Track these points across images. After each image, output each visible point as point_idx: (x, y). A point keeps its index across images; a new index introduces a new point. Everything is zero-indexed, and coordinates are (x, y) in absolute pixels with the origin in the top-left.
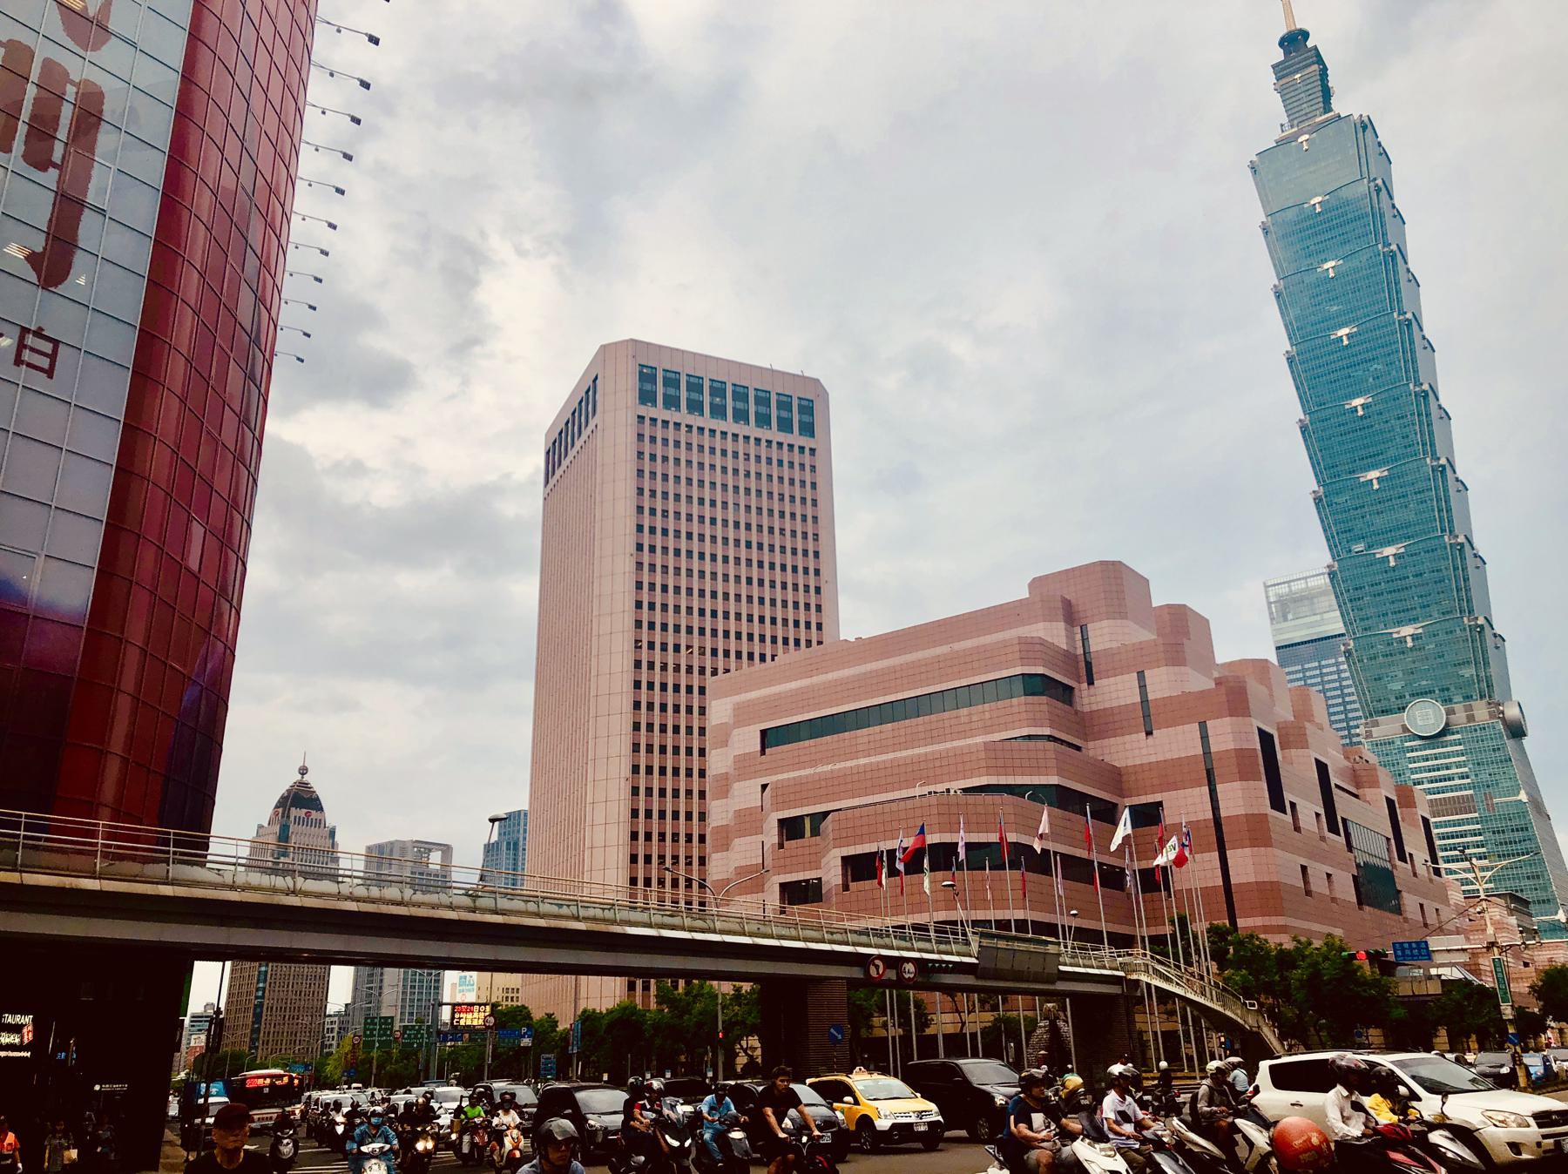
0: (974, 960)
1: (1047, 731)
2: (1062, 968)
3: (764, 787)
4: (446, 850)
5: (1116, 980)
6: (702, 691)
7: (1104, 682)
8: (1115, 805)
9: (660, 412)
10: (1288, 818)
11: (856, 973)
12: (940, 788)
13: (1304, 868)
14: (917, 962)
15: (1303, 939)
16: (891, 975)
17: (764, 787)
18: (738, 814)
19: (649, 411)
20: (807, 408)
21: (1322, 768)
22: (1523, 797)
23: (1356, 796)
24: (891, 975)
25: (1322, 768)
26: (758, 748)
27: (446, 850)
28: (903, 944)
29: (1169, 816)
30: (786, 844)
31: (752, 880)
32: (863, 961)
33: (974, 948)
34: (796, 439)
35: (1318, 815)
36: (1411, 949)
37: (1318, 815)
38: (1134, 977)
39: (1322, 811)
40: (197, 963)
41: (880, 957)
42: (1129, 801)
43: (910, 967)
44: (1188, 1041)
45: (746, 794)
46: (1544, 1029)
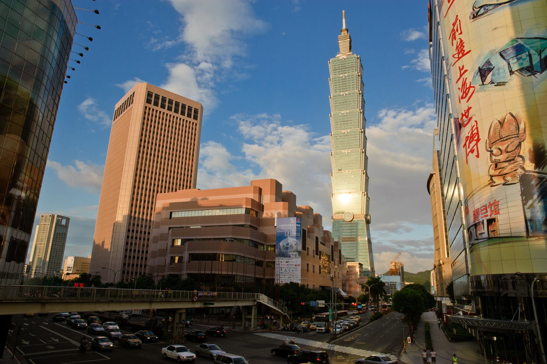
4: (68, 219)
9: (152, 106)
10: (306, 252)
19: (148, 105)
20: (196, 111)
21: (317, 238)
22: (366, 239)
25: (317, 238)
34: (192, 120)
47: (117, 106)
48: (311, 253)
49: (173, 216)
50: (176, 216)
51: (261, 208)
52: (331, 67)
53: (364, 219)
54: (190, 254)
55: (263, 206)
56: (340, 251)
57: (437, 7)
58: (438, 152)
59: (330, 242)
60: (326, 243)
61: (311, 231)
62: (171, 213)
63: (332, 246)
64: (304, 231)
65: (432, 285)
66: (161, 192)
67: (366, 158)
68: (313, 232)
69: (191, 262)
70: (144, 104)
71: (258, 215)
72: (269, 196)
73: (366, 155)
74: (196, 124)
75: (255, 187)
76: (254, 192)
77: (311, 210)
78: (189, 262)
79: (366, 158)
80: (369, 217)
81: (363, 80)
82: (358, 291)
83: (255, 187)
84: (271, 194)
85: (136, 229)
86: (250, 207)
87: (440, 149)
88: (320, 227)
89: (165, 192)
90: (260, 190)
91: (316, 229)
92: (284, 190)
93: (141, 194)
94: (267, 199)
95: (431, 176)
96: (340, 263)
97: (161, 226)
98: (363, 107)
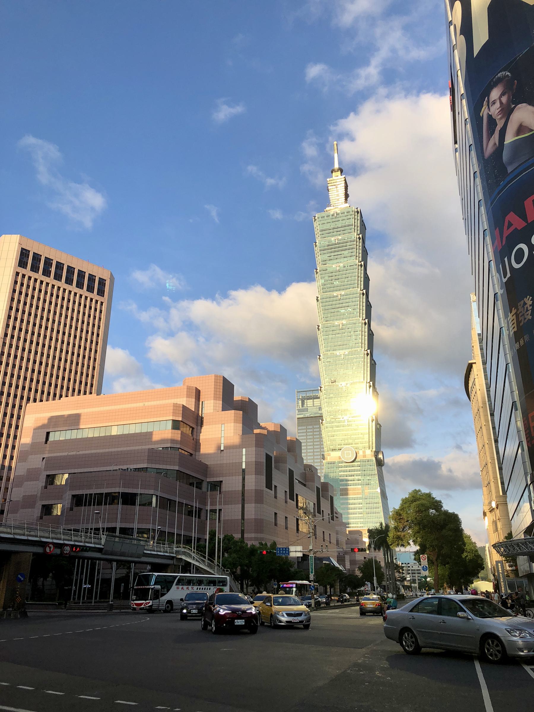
0: (102, 547)
1: (12, 477)
2: (145, 552)
3: (44, 458)
5: (173, 558)
6: (20, 407)
7: (208, 427)
8: (203, 481)
9: (28, 272)
11: (40, 550)
12: (125, 467)
13: (276, 514)
14: (72, 546)
15: (264, 543)
16: (58, 551)
17: (44, 458)
18: (29, 470)
19: (22, 271)
20: (102, 282)
21: (291, 473)
23: (305, 485)
24: (58, 551)
26: (44, 440)
28: (67, 537)
29: (224, 488)
30: (44, 517)
31: (28, 502)
32: (44, 545)
33: (103, 541)
34: (95, 296)
35: (286, 492)
36: (283, 550)
37: (286, 492)
38: (180, 557)
39: (288, 491)
40: (234, 399)
41: (53, 544)
42: (208, 480)
43: (68, 548)
44: (76, 585)
46: (364, 585)
48: (281, 495)
49: (51, 438)
50: (57, 439)
51: (199, 421)
53: (374, 459)
54: (74, 496)
55: (202, 418)
56: (332, 498)
57: (459, 71)
58: (479, 335)
59: (313, 481)
60: (307, 483)
61: (280, 460)
62: (48, 433)
63: (318, 489)
64: (268, 458)
65: (464, 101)
66: (35, 400)
68: (285, 462)
69: (44, 517)
70: (15, 268)
71: (195, 433)
72: (212, 401)
74: (102, 303)
75: (189, 388)
76: (188, 396)
77: (283, 430)
78: (71, 509)
80: (380, 456)
81: (372, 328)
83: (189, 388)
84: (215, 398)
86: (180, 419)
87: (480, 332)
88: (298, 458)
89: (41, 401)
90: (198, 393)
91: (290, 459)
92: (237, 397)
94: (210, 406)
95: (470, 367)
96: (333, 519)
97: (30, 457)
98: (368, 315)
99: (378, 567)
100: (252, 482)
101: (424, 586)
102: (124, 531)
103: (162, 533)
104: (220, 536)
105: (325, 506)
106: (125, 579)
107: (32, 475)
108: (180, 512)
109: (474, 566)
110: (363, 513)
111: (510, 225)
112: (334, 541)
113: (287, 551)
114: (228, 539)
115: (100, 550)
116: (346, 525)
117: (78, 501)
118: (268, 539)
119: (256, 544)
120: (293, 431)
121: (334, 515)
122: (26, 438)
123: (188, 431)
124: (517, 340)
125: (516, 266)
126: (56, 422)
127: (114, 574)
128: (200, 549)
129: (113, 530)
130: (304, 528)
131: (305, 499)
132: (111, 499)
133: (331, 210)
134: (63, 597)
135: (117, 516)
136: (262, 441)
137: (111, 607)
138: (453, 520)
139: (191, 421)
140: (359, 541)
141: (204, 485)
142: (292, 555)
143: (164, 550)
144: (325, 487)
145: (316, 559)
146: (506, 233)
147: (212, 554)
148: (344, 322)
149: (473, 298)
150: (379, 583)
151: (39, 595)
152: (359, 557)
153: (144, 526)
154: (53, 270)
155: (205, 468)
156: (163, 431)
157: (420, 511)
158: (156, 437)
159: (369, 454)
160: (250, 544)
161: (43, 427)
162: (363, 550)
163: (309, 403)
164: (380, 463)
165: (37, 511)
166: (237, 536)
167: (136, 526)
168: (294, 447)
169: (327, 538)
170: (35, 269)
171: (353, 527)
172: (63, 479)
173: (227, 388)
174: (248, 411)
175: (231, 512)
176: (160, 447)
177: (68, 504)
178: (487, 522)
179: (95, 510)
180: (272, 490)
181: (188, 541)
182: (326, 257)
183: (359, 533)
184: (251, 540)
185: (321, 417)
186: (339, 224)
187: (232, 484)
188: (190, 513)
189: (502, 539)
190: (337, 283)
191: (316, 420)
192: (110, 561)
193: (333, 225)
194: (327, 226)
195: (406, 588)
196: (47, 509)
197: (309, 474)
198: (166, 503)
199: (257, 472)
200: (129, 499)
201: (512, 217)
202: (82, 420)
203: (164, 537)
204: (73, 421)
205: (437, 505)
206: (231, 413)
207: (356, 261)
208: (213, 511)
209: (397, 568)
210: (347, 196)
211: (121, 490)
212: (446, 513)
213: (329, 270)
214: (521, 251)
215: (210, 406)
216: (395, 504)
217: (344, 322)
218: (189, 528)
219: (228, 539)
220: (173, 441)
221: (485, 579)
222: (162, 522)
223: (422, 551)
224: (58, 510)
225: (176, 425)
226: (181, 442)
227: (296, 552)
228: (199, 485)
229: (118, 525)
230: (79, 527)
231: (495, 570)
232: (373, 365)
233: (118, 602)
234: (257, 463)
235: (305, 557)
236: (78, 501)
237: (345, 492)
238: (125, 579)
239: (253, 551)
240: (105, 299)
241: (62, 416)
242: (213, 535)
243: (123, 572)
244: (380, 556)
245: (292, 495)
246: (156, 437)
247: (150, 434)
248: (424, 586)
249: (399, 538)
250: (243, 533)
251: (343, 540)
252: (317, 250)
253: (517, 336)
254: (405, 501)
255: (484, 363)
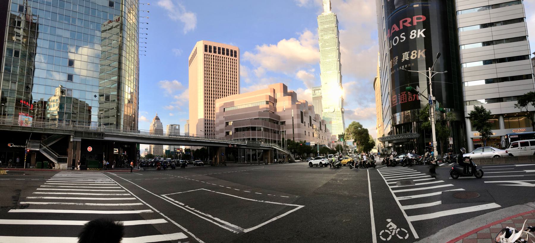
4: (179, 125)
9: (208, 53)
11: (227, 146)
19: (206, 53)
20: (235, 52)
21: (310, 117)
25: (310, 117)
27: (179, 125)
29: (286, 123)
31: (221, 131)
32: (228, 144)
45: (221, 118)
47: (190, 58)
48: (307, 124)
51: (275, 101)
52: (319, 21)
64: (302, 113)
67: (340, 65)
73: (340, 63)
75: (271, 89)
76: (271, 92)
79: (340, 65)
82: (337, 138)
84: (281, 92)
85: (208, 125)
88: (313, 112)
90: (274, 90)
92: (289, 90)
93: (209, 105)
94: (279, 95)
95: (376, 79)
99: (341, 147)
100: (297, 121)
101: (355, 152)
102: (253, 139)
103: (266, 140)
104: (286, 139)
105: (323, 128)
106: (255, 155)
107: (221, 123)
108: (271, 132)
109: (372, 145)
110: (337, 128)
111: (394, 29)
112: (326, 139)
113: (309, 143)
114: (289, 140)
115: (246, 146)
116: (331, 133)
117: (237, 130)
118: (303, 140)
119: (299, 142)
120: (310, 102)
121: (326, 130)
122: (217, 111)
123: (272, 104)
124: (392, 71)
125: (394, 45)
126: (226, 104)
127: (251, 153)
128: (279, 144)
129: (249, 139)
130: (315, 135)
131: (316, 125)
132: (248, 129)
133: (324, 14)
134: (236, 160)
135: (250, 135)
136: (298, 106)
137: (252, 163)
138: (366, 131)
139: (273, 101)
140: (335, 139)
141: (279, 123)
142: (311, 145)
143: (267, 145)
144: (323, 121)
145: (320, 145)
146: (392, 32)
147: (283, 146)
148: (330, 60)
149: (379, 54)
150: (341, 152)
151: (229, 159)
152: (335, 144)
153: (259, 137)
154: (217, 50)
155: (279, 117)
156: (263, 106)
157: (355, 129)
158: (260, 107)
159: (340, 110)
160: (296, 142)
161: (222, 106)
162: (335, 142)
163: (317, 91)
164: (343, 112)
165: (224, 134)
166: (292, 139)
167: (257, 137)
168: (311, 108)
169: (324, 138)
170: (215, 52)
171: (333, 134)
172: (231, 123)
173: (285, 88)
174: (293, 96)
175: (289, 131)
176: (262, 111)
177: (234, 131)
178: (377, 131)
179: (242, 133)
180: (405, 210)
181: (275, 142)
182: (323, 33)
183: (335, 136)
184: (297, 140)
185: (321, 97)
186: (328, 20)
187: (289, 122)
188: (275, 133)
189: (381, 136)
190: (327, 44)
191: (319, 98)
192: (250, 149)
193: (325, 20)
194: (323, 21)
195: (351, 153)
196: (227, 133)
197: (317, 117)
198: (266, 130)
199: (298, 118)
200: (254, 129)
201: (395, 26)
202: (235, 103)
203: (266, 141)
204: (232, 104)
205: (361, 126)
206: (287, 97)
207: (334, 35)
208: (283, 131)
209: (347, 147)
210: (331, 8)
211: (251, 126)
212: (363, 129)
213: (324, 39)
214: (396, 39)
215: (279, 95)
216: (347, 126)
217: (330, 60)
218: (275, 137)
219: (289, 140)
220: (267, 108)
221: (375, 148)
222: (266, 136)
223: (355, 141)
224: (231, 133)
225: (267, 103)
226: (270, 109)
227: (312, 144)
228: (277, 123)
229: (251, 137)
230: (239, 138)
231: (378, 146)
232: (341, 77)
233: (253, 162)
234: (298, 115)
235: (316, 145)
236: (237, 130)
237: (330, 123)
238: (255, 155)
239: (298, 144)
240: (237, 58)
241: (228, 103)
242: (283, 139)
243: (254, 152)
244: (342, 143)
245: (311, 125)
246: (260, 107)
247: (259, 106)
248: (355, 152)
249: (348, 137)
250: (294, 138)
251: (330, 138)
252: (319, 31)
253: (392, 70)
254: (350, 125)
255: (381, 78)
